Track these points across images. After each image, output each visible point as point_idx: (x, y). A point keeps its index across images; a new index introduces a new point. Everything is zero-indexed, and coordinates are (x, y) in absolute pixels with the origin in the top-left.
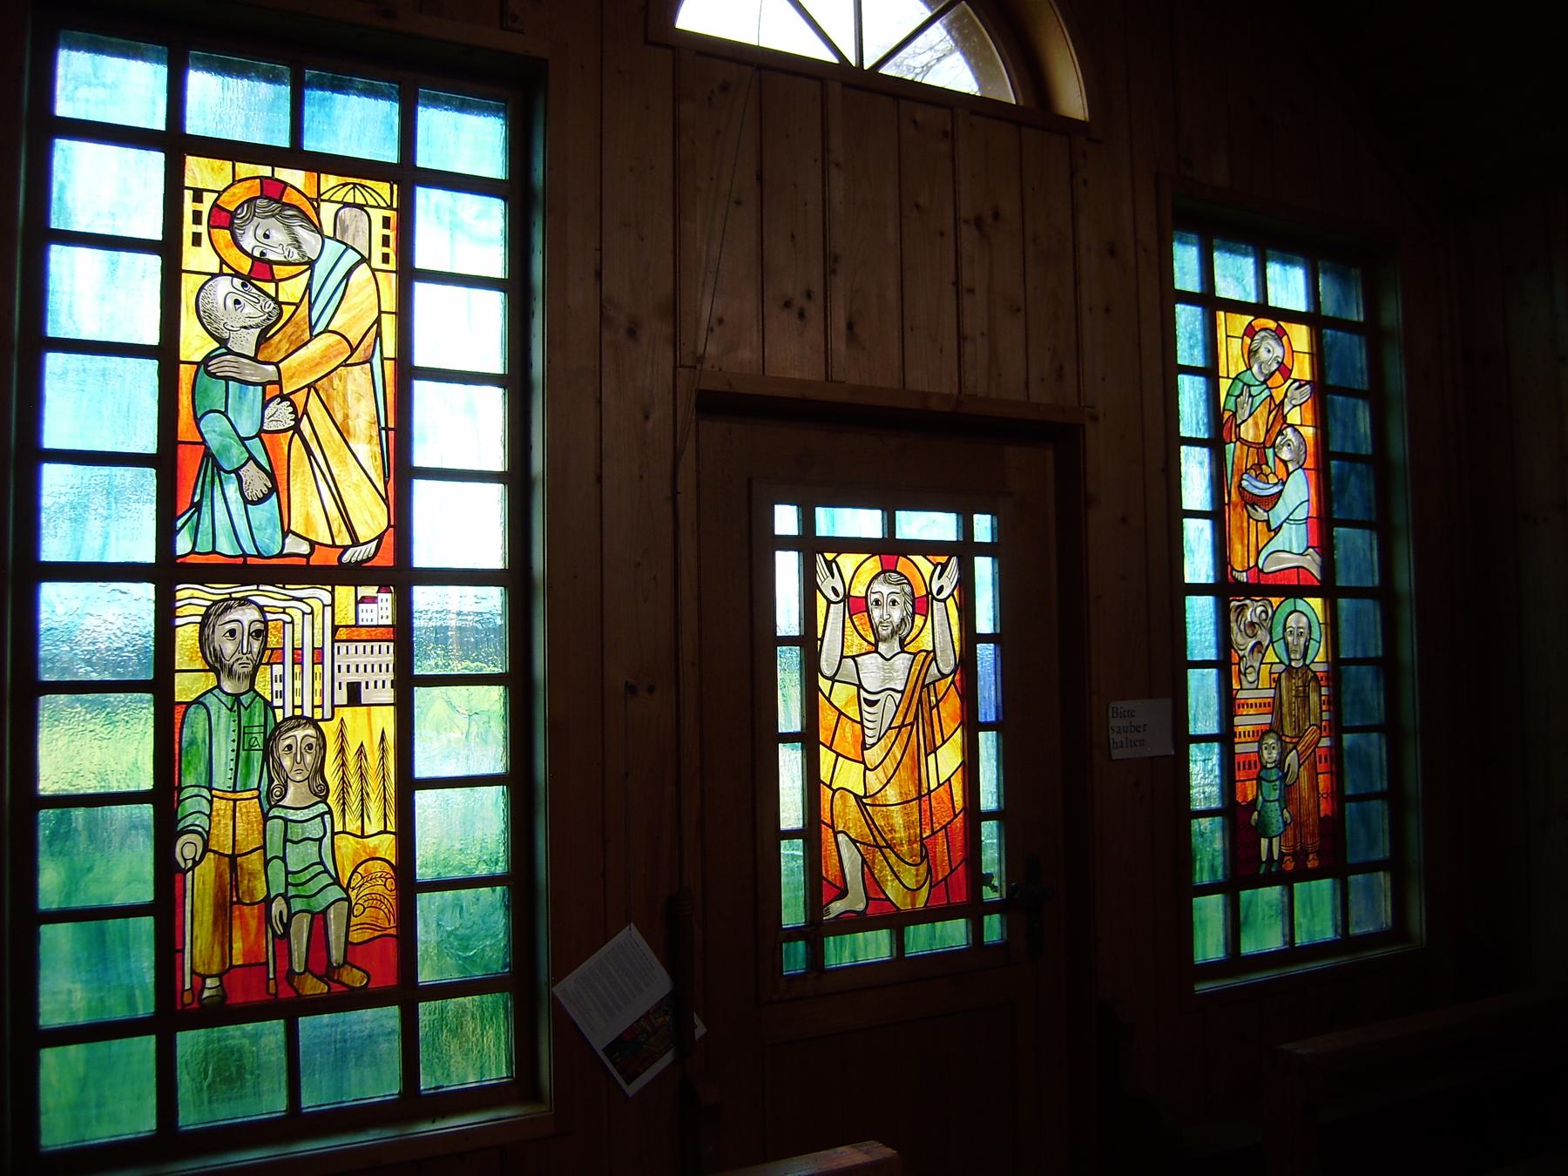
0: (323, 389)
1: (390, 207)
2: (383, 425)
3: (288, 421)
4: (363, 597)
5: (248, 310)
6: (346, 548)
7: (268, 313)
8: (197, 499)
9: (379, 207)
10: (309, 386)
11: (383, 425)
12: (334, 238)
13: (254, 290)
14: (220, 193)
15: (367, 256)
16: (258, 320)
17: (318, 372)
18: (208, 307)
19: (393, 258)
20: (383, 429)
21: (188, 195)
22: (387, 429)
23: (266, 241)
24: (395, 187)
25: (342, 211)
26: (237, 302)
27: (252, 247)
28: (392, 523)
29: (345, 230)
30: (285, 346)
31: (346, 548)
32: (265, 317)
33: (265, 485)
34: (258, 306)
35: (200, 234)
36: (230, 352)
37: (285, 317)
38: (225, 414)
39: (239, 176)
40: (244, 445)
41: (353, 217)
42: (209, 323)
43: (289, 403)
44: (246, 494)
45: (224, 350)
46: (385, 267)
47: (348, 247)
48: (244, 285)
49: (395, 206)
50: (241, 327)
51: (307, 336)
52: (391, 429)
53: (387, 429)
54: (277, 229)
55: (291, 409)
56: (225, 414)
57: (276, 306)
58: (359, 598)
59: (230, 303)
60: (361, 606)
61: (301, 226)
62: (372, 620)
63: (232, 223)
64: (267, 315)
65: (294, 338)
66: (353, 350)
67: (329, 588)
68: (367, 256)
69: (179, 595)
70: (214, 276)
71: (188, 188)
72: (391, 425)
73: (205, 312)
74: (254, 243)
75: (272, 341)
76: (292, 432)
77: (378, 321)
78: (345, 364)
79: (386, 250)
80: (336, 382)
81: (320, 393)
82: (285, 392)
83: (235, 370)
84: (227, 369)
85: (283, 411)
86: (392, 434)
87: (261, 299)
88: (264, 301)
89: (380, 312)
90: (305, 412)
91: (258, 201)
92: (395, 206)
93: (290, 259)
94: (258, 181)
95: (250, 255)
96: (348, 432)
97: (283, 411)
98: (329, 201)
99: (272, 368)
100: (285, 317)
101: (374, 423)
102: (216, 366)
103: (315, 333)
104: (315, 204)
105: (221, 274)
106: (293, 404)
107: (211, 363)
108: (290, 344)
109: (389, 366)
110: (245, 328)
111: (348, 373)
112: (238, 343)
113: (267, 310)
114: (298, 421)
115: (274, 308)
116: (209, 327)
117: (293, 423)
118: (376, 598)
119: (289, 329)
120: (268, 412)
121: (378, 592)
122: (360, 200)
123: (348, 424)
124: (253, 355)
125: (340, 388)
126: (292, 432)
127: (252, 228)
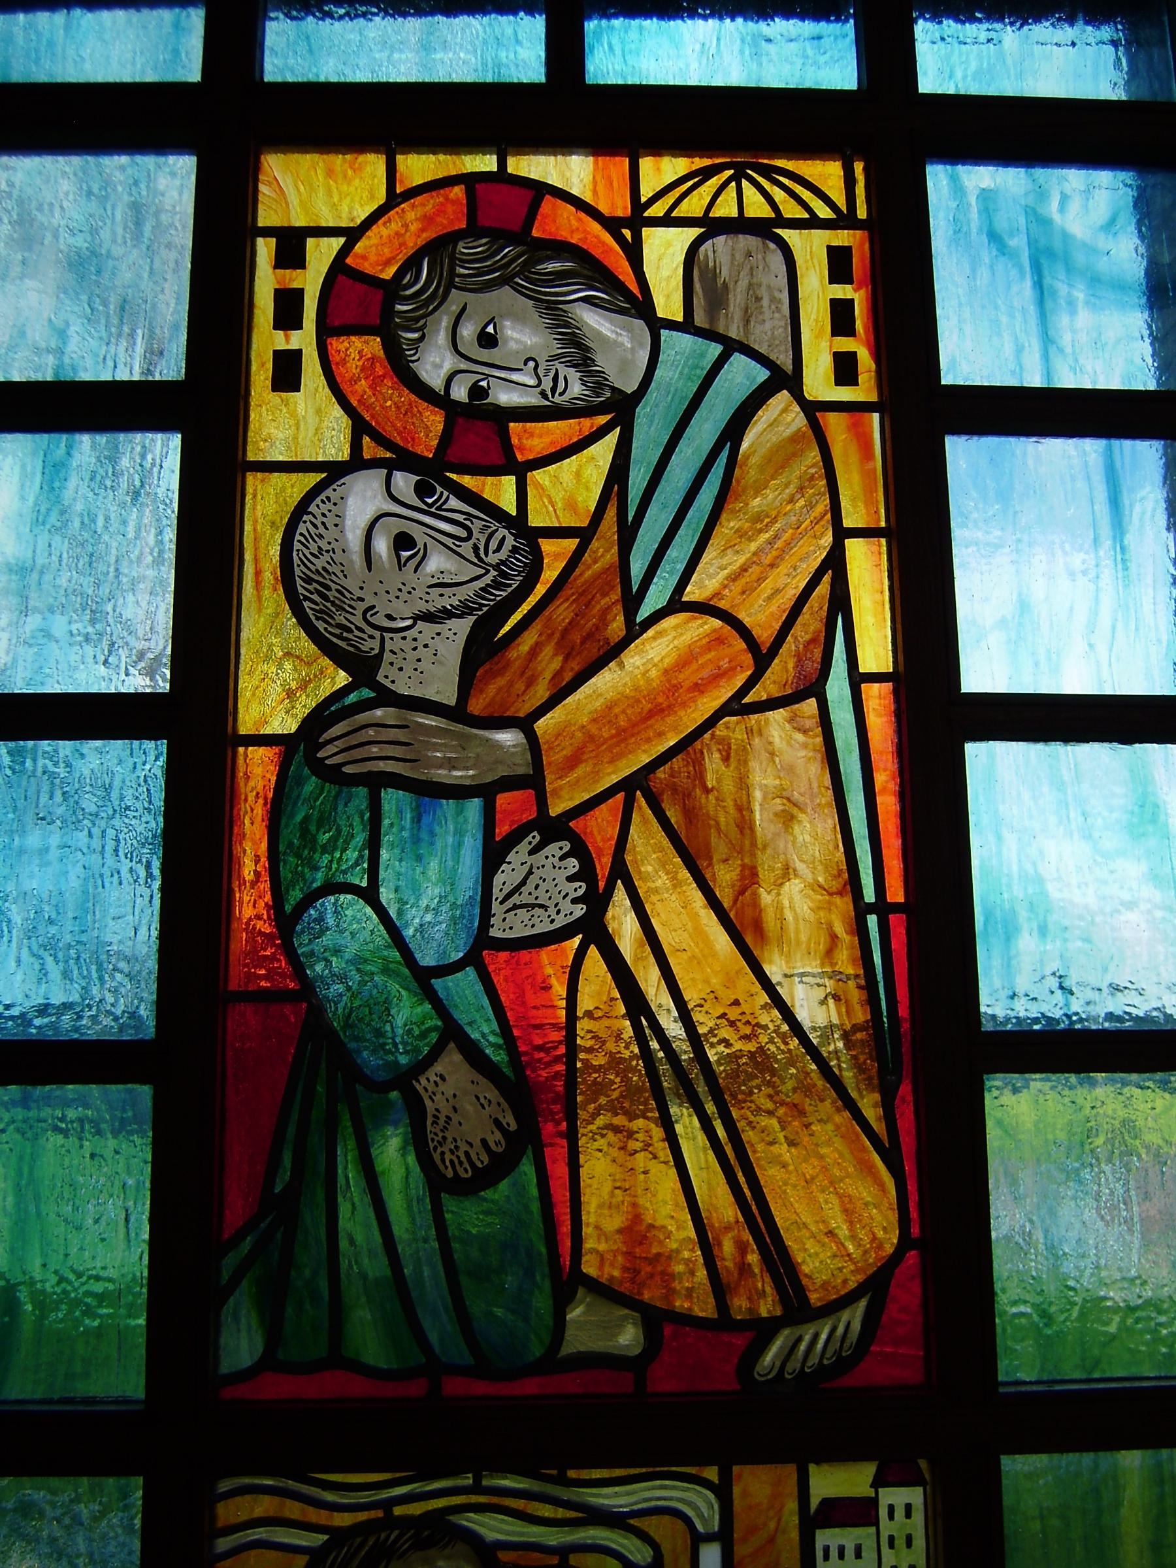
0: (675, 790)
1: (844, 220)
2: (869, 895)
3: (566, 906)
4: (826, 1503)
5: (437, 563)
6: (765, 1330)
7: (496, 567)
8: (284, 1177)
9: (813, 222)
10: (628, 785)
11: (869, 895)
12: (686, 326)
13: (454, 503)
14: (353, 234)
15: (788, 366)
16: (469, 591)
17: (660, 734)
18: (319, 564)
19: (865, 359)
20: (871, 909)
21: (265, 249)
22: (882, 907)
23: (485, 355)
24: (859, 167)
25: (707, 246)
26: (403, 542)
27: (444, 372)
28: (915, 1231)
29: (718, 299)
30: (550, 664)
31: (765, 1330)
32: (488, 579)
33: (497, 1123)
34: (466, 549)
35: (298, 353)
36: (387, 697)
37: (550, 574)
38: (370, 895)
39: (402, 182)
40: (431, 996)
41: (739, 257)
42: (322, 614)
43: (566, 846)
44: (437, 1157)
45: (367, 693)
46: (845, 394)
47: (731, 347)
48: (422, 490)
49: (862, 213)
50: (416, 618)
51: (617, 626)
52: (896, 908)
53: (882, 907)
54: (520, 319)
55: (573, 865)
56: (370, 895)
57: (521, 543)
58: (814, 1502)
59: (382, 546)
60: (824, 1538)
61: (584, 300)
62: (318, 506)
63: (388, 312)
64: (493, 573)
65: (576, 637)
66: (763, 658)
67: (712, 1473)
68: (788, 366)
69: (228, 1512)
70: (334, 472)
71: (267, 232)
72: (896, 894)
73: (308, 580)
74: (449, 362)
75: (513, 654)
76: (576, 941)
77: (835, 562)
78: (736, 706)
79: (846, 344)
80: (713, 764)
81: (666, 805)
82: (555, 810)
83: (397, 751)
84: (375, 750)
85: (547, 872)
86: (897, 921)
87: (476, 526)
88: (482, 530)
89: (841, 534)
90: (621, 871)
91: (461, 248)
92: (862, 213)
93: (557, 399)
94: (458, 191)
95: (440, 400)
96: (758, 927)
97: (547, 872)
98: (667, 221)
99: (508, 738)
100: (550, 574)
101: (840, 893)
102: (340, 744)
103: (645, 612)
104: (627, 233)
105: (356, 463)
106: (580, 850)
107: (326, 736)
108: (566, 659)
109: (877, 697)
110: (428, 617)
111: (749, 731)
112: (409, 670)
113: (493, 559)
114: (597, 902)
115: (515, 550)
116: (321, 626)
117: (579, 910)
118: (873, 1502)
119: (562, 612)
120: (505, 878)
121: (878, 1483)
122: (757, 207)
123: (755, 903)
124: (452, 701)
125: (728, 786)
126: (576, 941)
127: (445, 322)
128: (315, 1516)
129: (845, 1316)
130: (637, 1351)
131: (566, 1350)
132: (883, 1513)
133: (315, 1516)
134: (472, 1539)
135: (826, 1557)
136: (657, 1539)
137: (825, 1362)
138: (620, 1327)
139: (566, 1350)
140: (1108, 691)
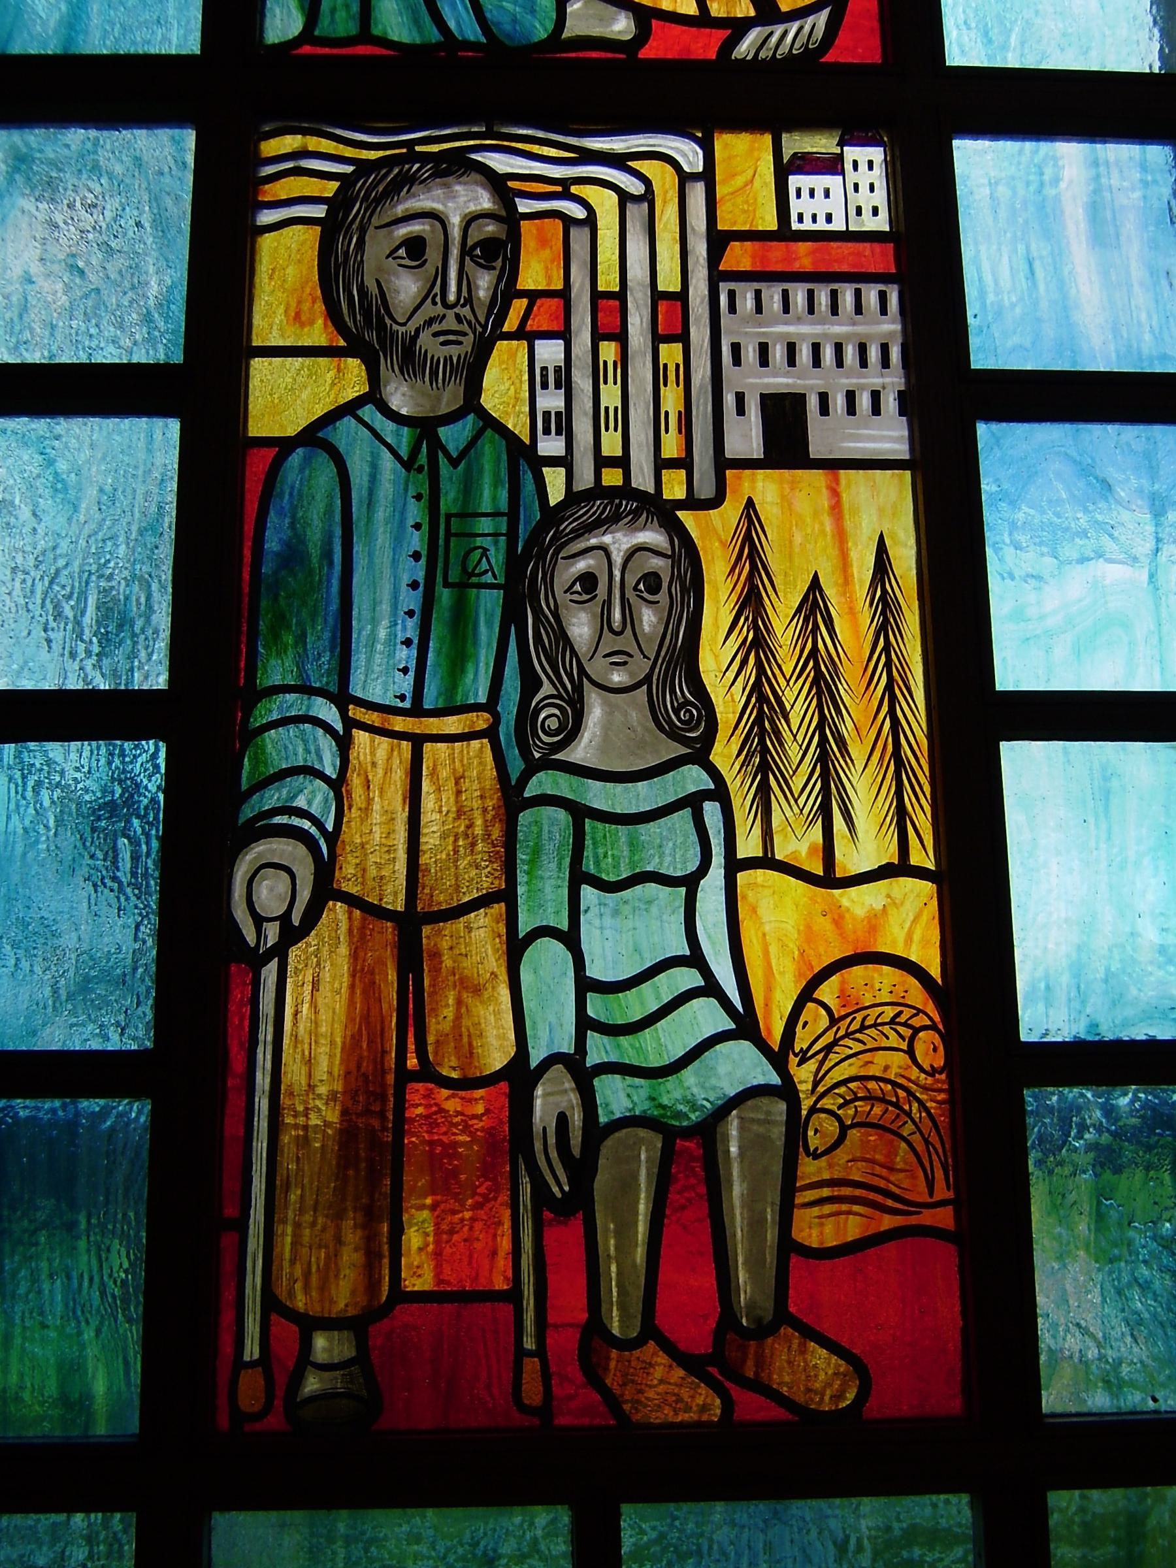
31: (739, 27)
118: (840, 157)
128: (349, 152)
129: (810, 20)
130: (629, 37)
131: (566, 34)
132: (848, 166)
133: (349, 152)
134: (486, 171)
135: (799, 196)
136: (627, 894)
137: (794, 52)
138: (614, 20)
139: (566, 34)
140: (1012, 61)
